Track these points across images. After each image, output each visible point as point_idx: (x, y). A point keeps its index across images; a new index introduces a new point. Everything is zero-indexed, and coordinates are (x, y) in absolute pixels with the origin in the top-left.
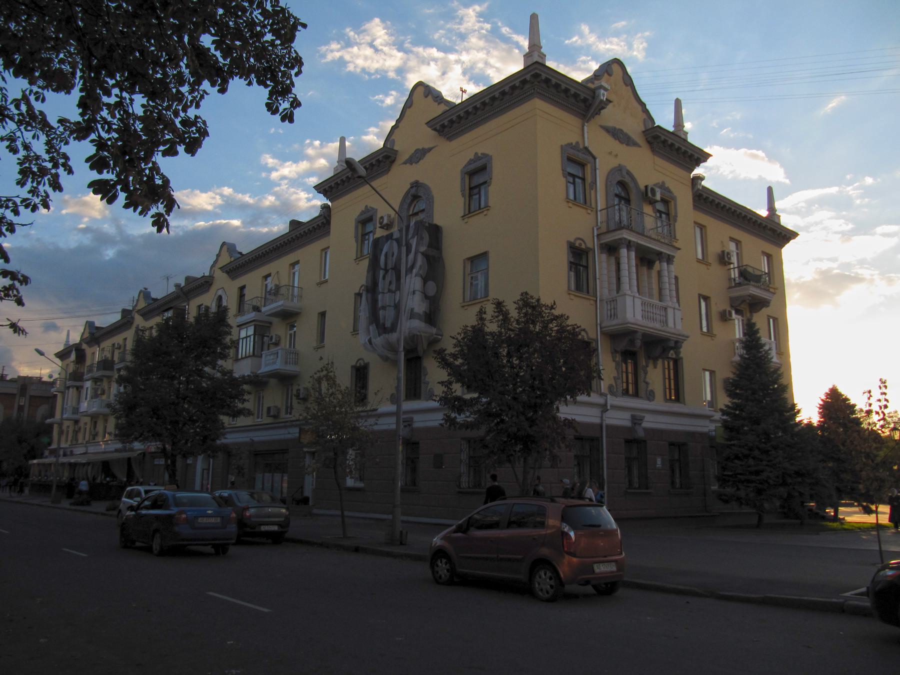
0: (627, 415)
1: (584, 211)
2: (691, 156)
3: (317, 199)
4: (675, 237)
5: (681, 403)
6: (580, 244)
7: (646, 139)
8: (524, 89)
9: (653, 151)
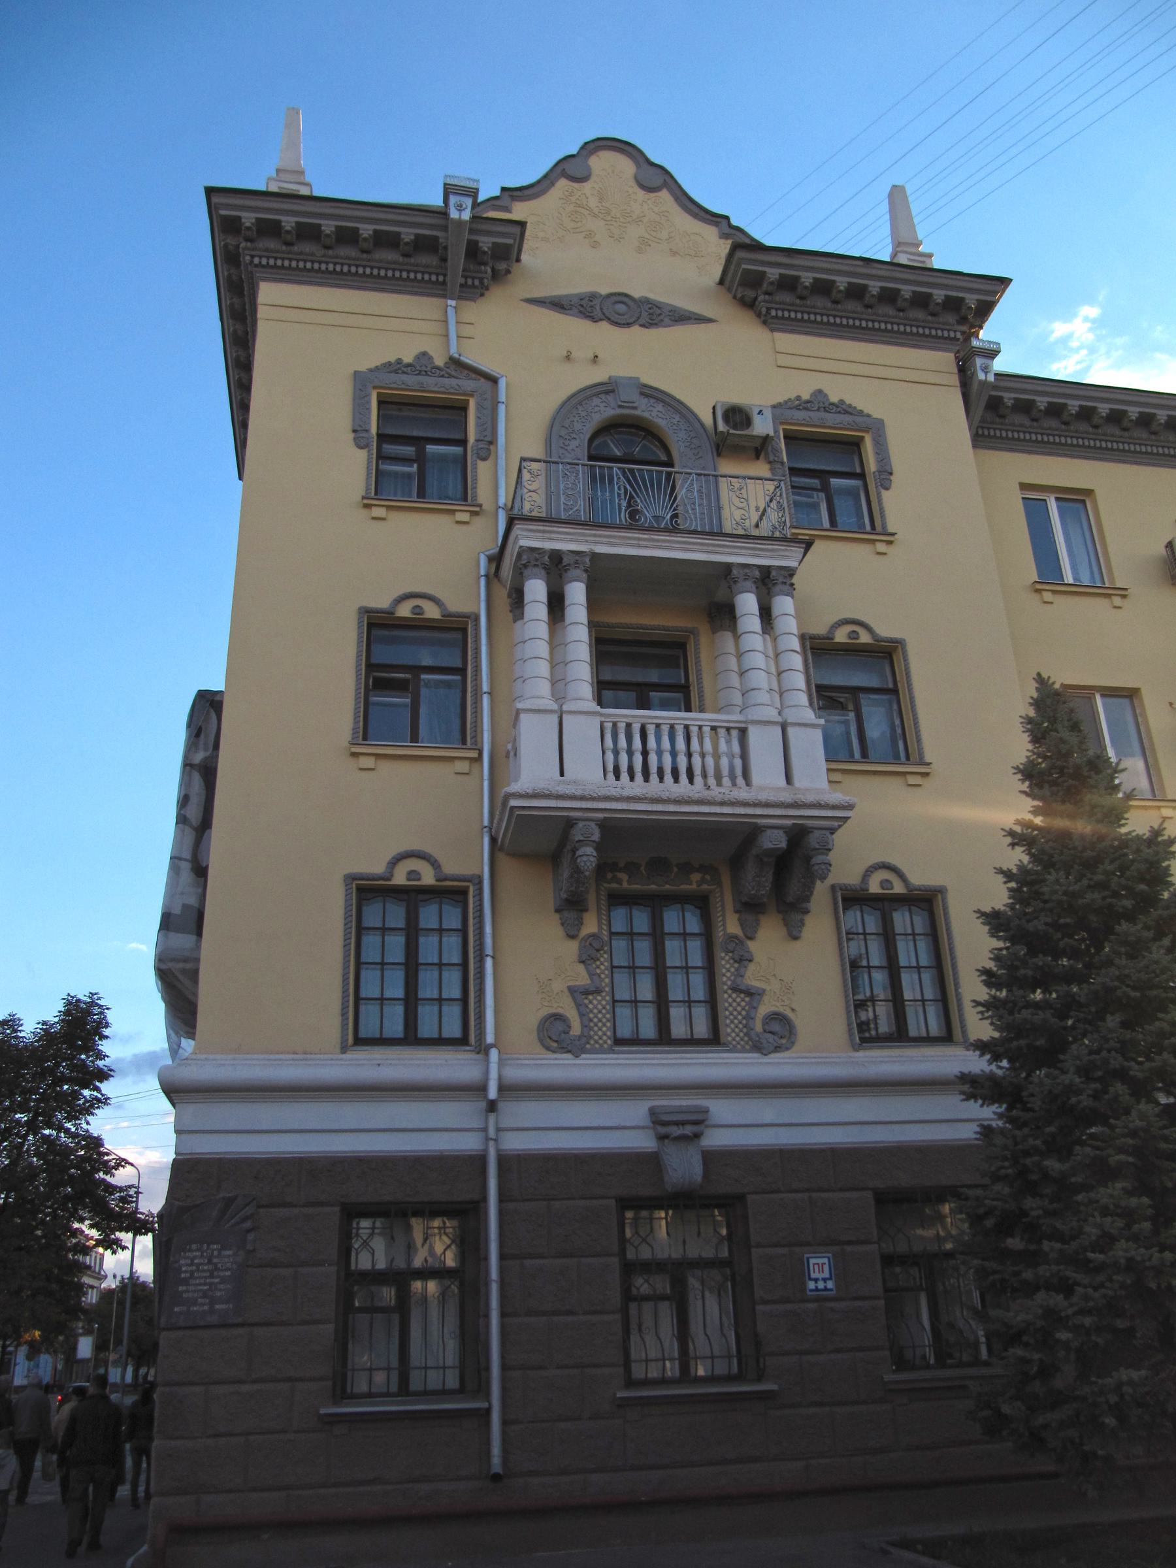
0: (636, 1111)
1: (444, 519)
2: (953, 305)
3: (29, 1351)
4: (884, 525)
5: (957, 1044)
6: (854, 635)
7: (735, 297)
8: (296, 248)
9: (769, 321)
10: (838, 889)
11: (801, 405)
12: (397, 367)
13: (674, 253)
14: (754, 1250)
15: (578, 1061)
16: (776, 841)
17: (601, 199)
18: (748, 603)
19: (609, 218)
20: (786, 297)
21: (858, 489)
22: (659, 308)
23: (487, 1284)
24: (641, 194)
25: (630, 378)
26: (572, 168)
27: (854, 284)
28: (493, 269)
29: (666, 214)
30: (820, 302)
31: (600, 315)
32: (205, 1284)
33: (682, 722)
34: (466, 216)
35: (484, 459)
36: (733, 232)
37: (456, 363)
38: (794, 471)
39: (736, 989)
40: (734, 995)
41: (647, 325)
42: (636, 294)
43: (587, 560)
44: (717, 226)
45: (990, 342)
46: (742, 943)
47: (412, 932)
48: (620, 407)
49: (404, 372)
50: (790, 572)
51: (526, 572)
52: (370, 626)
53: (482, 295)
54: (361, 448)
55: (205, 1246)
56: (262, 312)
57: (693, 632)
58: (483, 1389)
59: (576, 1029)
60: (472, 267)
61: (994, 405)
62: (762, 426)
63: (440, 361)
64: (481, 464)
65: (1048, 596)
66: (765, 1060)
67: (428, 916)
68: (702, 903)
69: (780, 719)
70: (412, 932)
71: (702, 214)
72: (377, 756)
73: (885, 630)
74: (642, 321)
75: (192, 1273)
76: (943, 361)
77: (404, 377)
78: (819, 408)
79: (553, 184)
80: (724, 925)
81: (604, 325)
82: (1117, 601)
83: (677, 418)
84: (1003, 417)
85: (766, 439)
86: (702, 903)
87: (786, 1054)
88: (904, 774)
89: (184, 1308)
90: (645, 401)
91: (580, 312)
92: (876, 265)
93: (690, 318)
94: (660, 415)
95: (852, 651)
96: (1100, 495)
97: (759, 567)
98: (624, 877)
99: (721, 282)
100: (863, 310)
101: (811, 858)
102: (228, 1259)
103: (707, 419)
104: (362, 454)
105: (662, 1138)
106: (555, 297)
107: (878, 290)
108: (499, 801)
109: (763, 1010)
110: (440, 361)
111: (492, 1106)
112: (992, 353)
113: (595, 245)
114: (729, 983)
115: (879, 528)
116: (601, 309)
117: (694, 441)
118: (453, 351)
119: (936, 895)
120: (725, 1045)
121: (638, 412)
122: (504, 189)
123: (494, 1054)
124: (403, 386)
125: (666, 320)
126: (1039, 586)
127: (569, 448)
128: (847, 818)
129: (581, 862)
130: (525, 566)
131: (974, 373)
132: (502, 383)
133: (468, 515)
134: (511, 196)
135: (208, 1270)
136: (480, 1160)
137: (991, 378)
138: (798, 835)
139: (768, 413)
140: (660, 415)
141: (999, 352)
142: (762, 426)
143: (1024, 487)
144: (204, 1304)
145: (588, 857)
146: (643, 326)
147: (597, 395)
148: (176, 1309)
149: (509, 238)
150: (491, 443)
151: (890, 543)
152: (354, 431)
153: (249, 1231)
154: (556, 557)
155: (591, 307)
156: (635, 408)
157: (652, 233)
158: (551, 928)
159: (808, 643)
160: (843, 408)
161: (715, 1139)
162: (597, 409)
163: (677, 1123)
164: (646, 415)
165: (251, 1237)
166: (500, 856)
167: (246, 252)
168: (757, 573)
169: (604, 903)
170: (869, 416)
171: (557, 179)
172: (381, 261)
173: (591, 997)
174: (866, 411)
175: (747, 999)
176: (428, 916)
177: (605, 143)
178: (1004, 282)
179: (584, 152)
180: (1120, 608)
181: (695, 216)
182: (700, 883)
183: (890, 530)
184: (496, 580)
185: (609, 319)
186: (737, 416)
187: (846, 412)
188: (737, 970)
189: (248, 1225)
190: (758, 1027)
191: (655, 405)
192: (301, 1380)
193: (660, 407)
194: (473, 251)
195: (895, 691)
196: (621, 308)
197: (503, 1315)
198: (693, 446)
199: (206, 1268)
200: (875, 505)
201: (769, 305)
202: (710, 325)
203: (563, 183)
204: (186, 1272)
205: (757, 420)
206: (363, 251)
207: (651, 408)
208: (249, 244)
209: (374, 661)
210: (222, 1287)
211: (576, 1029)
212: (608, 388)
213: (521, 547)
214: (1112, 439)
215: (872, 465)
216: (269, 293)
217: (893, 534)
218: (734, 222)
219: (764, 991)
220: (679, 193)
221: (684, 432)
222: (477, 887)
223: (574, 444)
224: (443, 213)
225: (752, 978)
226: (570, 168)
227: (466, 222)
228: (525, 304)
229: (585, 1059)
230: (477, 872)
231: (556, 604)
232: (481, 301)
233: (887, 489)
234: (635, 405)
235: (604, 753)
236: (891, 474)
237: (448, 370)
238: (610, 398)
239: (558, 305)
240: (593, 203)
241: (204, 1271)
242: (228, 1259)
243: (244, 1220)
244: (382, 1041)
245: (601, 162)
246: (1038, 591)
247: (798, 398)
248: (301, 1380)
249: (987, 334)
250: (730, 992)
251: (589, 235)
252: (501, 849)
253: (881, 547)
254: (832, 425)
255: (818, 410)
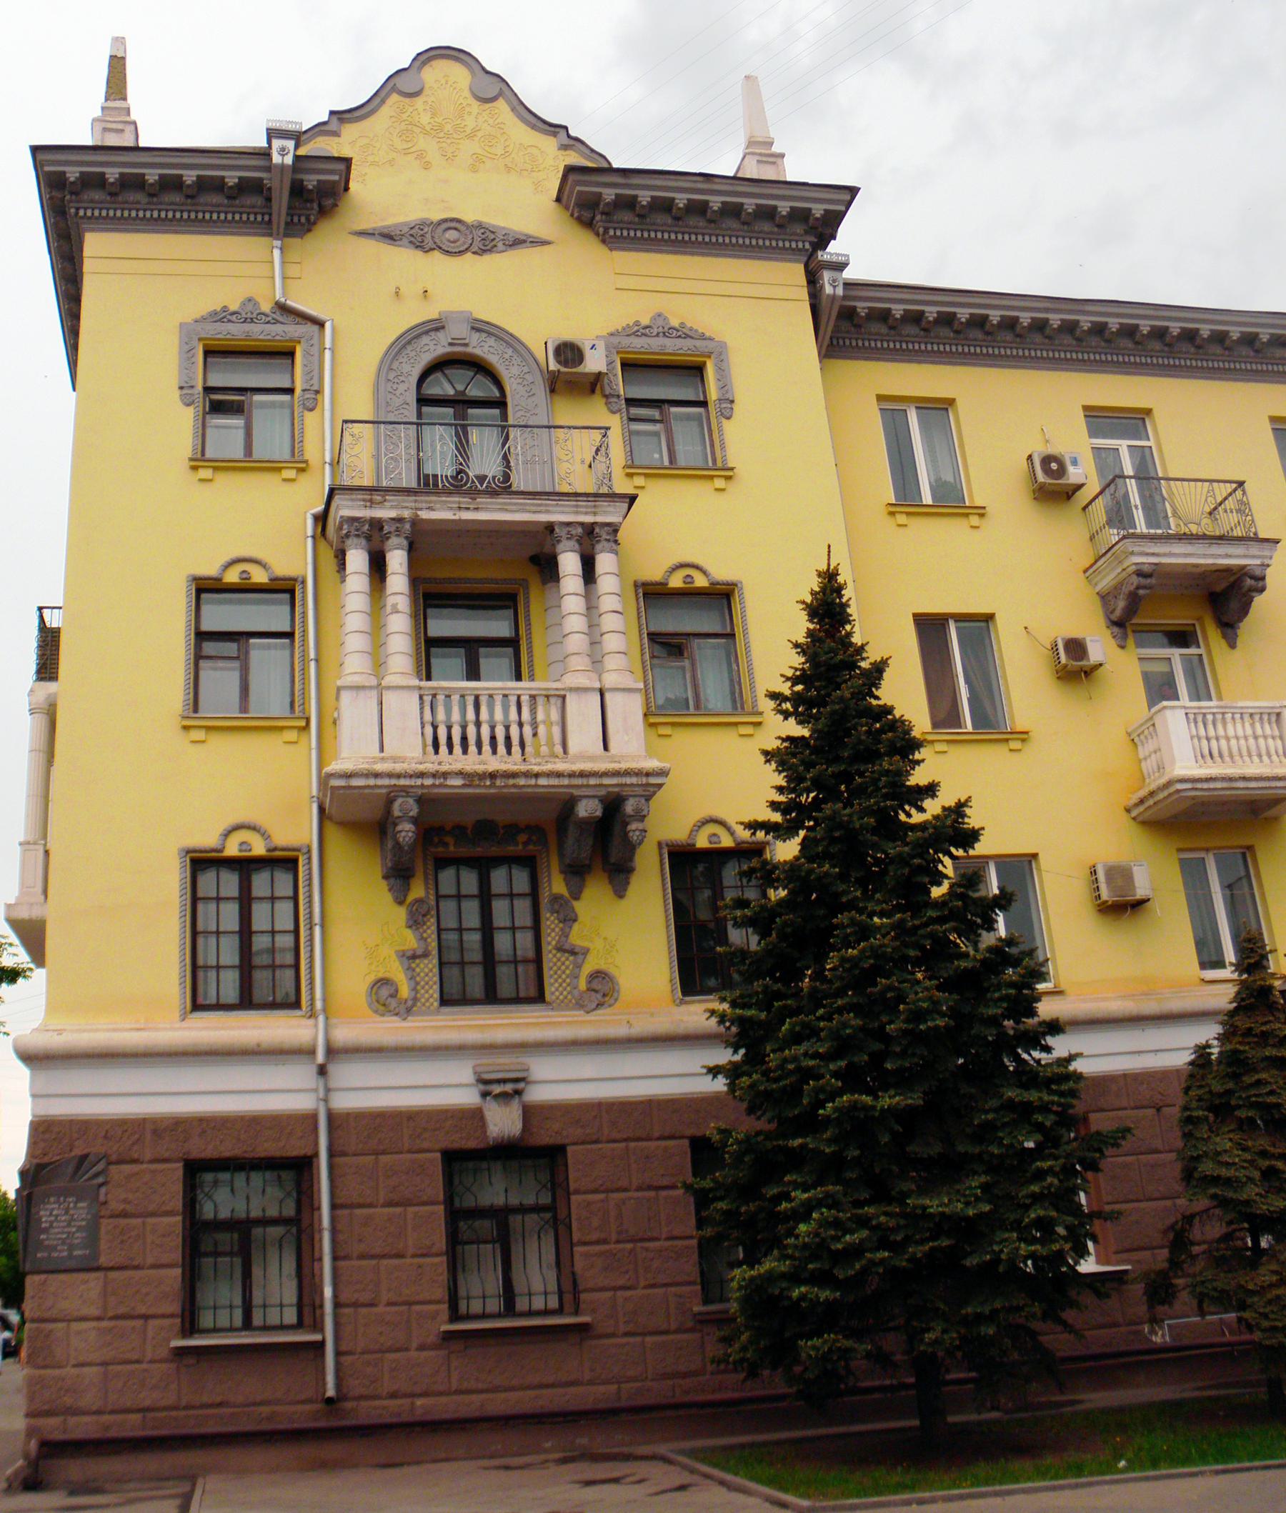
4: (724, 460)
7: (572, 215)
8: (120, 198)
9: (610, 241)
10: (664, 846)
11: (641, 331)
12: (222, 316)
13: (508, 169)
14: (573, 1198)
15: (405, 1024)
16: (587, 809)
17: (434, 115)
18: (569, 563)
19: (442, 135)
20: (626, 216)
21: (701, 414)
22: (493, 232)
23: (321, 1231)
24: (475, 104)
25: (462, 312)
26: (404, 83)
27: (694, 200)
28: (320, 205)
29: (502, 126)
30: (661, 218)
31: (431, 245)
32: (63, 1233)
33: (500, 692)
34: (289, 160)
35: (311, 410)
36: (572, 142)
37: (283, 308)
38: (631, 402)
39: (560, 949)
40: (559, 955)
41: (479, 251)
42: (469, 217)
43: (408, 526)
44: (555, 136)
45: (838, 255)
46: (567, 902)
47: (245, 901)
48: (451, 344)
49: (229, 321)
50: (614, 529)
51: (349, 542)
52: (199, 591)
53: (309, 230)
54: (188, 405)
55: (62, 1199)
56: (88, 266)
57: (525, 584)
58: (318, 1326)
59: (405, 991)
60: (297, 204)
61: (847, 314)
62: (595, 362)
63: (266, 307)
64: (308, 415)
65: (902, 519)
66: (591, 1017)
67: (260, 883)
68: (530, 863)
69: (597, 685)
70: (245, 901)
71: (540, 124)
72: (208, 728)
73: (722, 572)
74: (475, 248)
75: (51, 1223)
76: (795, 272)
77: (230, 327)
78: (658, 334)
79: (383, 102)
80: (550, 885)
81: (436, 253)
82: (974, 520)
83: (510, 351)
84: (858, 326)
85: (598, 376)
86: (530, 863)
87: (609, 1010)
88: (736, 724)
89: (46, 1254)
90: (476, 336)
91: (411, 242)
92: (717, 180)
93: (525, 241)
94: (491, 350)
95: (689, 595)
96: (959, 403)
97: (582, 524)
98: (449, 839)
99: (558, 200)
100: (705, 224)
101: (627, 824)
102: (82, 1210)
103: (540, 355)
104: (190, 412)
105: (485, 1095)
106: (384, 227)
107: (720, 205)
108: (324, 780)
109: (588, 968)
110: (266, 307)
111: (322, 1071)
112: (840, 266)
113: (427, 166)
114: (554, 943)
115: (719, 464)
116: (433, 237)
117: (527, 376)
118: (278, 295)
119: (765, 848)
120: (549, 1004)
121: (469, 350)
122: (332, 113)
123: (321, 1019)
124: (228, 337)
125: (500, 245)
126: (893, 509)
127: (398, 393)
128: (660, 786)
129: (401, 837)
130: (347, 536)
131: (822, 287)
132: (328, 325)
133: (294, 472)
134: (339, 119)
135: (65, 1221)
136: (312, 1118)
137: (840, 291)
138: (613, 805)
139: (601, 345)
140: (491, 350)
141: (847, 264)
142: (595, 362)
143: (880, 398)
144: (63, 1251)
145: (406, 831)
146: (474, 253)
147: (427, 332)
148: (39, 1255)
149: (335, 174)
150: (317, 392)
151: (728, 478)
152: (181, 388)
153: (101, 1185)
154: (377, 524)
155: (422, 236)
156: (466, 345)
157: (487, 148)
158: (380, 893)
159: (641, 591)
160: (683, 333)
161: (538, 1094)
162: (426, 348)
163: (499, 1081)
164: (478, 352)
165: (103, 1190)
166: (328, 824)
167: (71, 205)
168: (580, 530)
169: (431, 867)
170: (711, 339)
171: (388, 95)
172: (206, 205)
173: (417, 961)
174: (707, 334)
175: (571, 958)
176: (260, 883)
177: (438, 52)
178: (853, 191)
179: (417, 63)
180: (978, 527)
181: (533, 127)
182: (526, 844)
183: (730, 465)
184: (322, 540)
185: (440, 248)
186: (569, 352)
187: (687, 336)
188: (562, 929)
189: (100, 1180)
190: (583, 985)
191: (487, 339)
192: (154, 1317)
193: (491, 341)
194: (298, 190)
195: (732, 636)
196: (452, 235)
197: (335, 1258)
198: (525, 383)
199: (63, 1218)
200: (715, 436)
201: (606, 225)
202: (546, 248)
203: (395, 97)
204: (46, 1222)
205: (588, 354)
206: (188, 197)
207: (483, 344)
208: (74, 197)
209: (206, 626)
210: (78, 1235)
211: (405, 991)
212: (435, 326)
213: (341, 517)
214: (975, 343)
215: (713, 394)
216: (96, 245)
217: (732, 469)
218: (572, 133)
219: (588, 950)
220: (515, 103)
221: (516, 367)
222: (306, 856)
223: (402, 387)
224: (265, 154)
225: (577, 937)
226: (400, 82)
227: (288, 166)
228: (355, 237)
229: (413, 1022)
230: (307, 842)
231: (378, 566)
232: (309, 235)
233: (728, 418)
234: (466, 341)
235: (423, 727)
236: (732, 402)
237: (274, 316)
238: (440, 335)
239: (388, 236)
240: (425, 119)
241: (60, 1221)
242: (82, 1210)
243: (96, 1175)
244: (219, 1007)
245: (433, 74)
246: (892, 514)
247: (637, 323)
248: (154, 1317)
249: (835, 248)
250: (554, 952)
251: (420, 156)
252: (330, 818)
253: (719, 483)
254: (672, 348)
255: (658, 335)
